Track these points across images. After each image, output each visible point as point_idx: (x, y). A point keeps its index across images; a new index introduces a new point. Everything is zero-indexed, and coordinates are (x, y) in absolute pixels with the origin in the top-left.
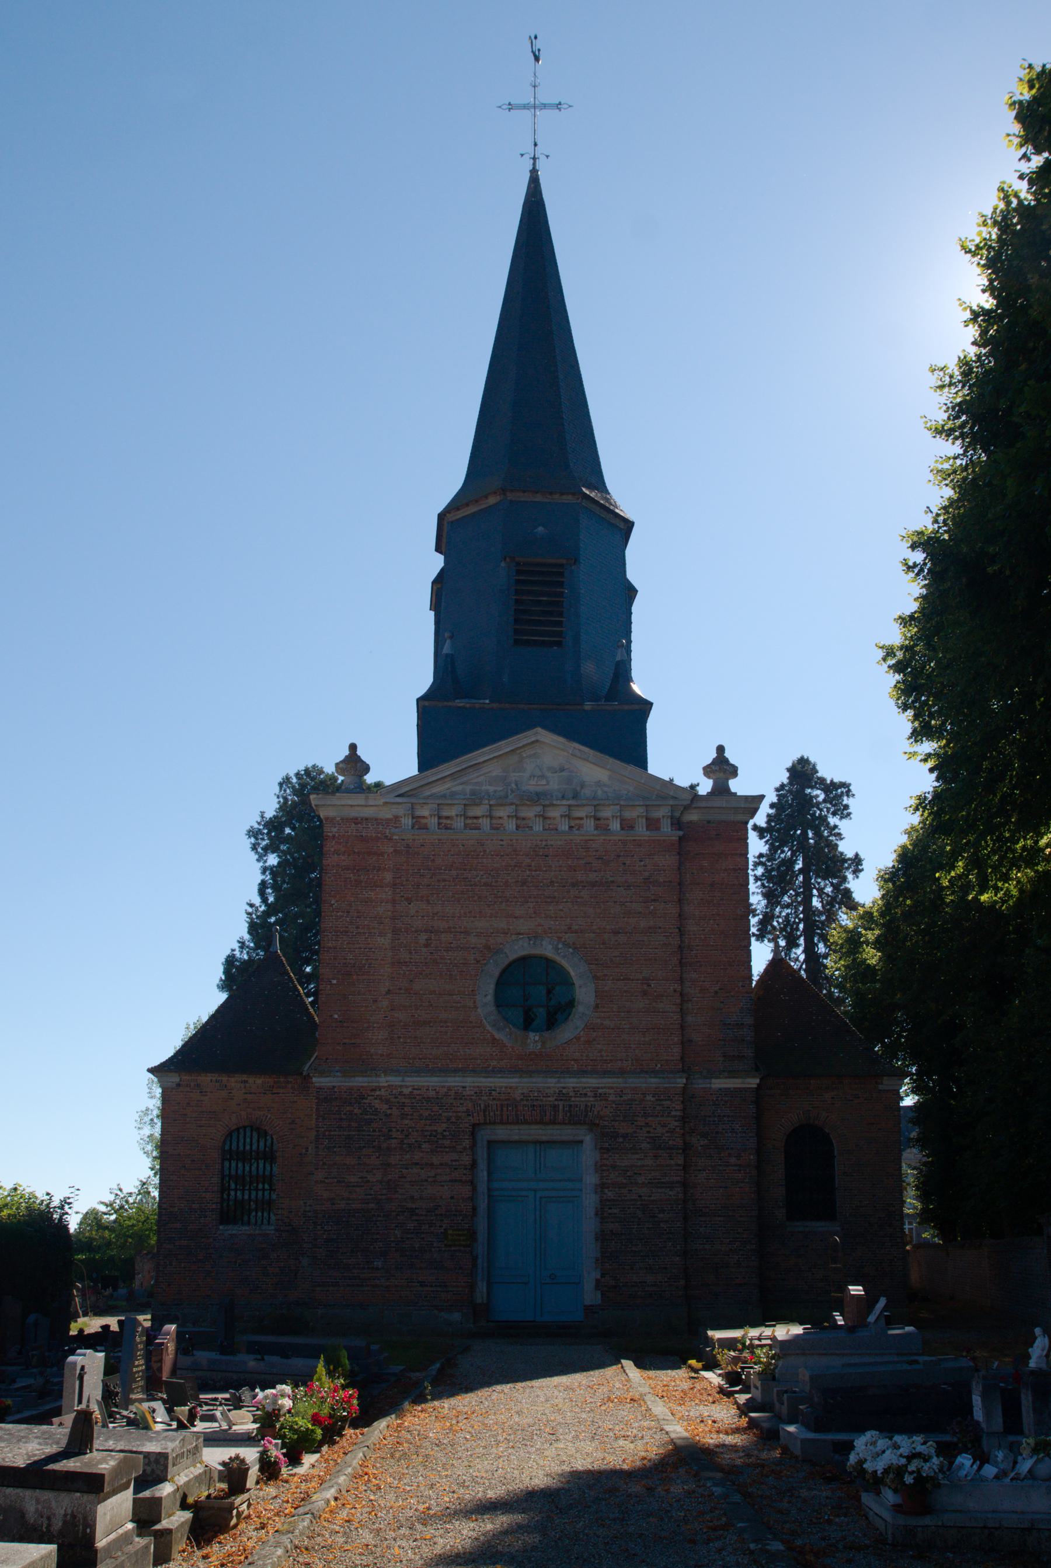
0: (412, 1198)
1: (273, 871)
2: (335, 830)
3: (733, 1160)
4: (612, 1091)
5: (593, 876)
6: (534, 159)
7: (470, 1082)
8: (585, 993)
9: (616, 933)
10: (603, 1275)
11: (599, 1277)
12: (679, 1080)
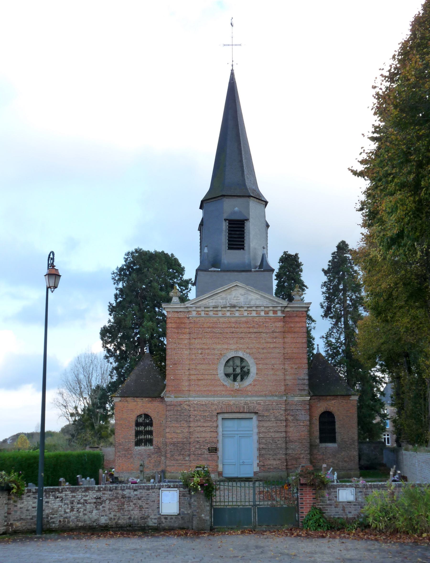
0: (198, 437)
1: (121, 290)
2: (170, 315)
3: (302, 424)
4: (262, 402)
5: (255, 330)
6: (232, 65)
7: (216, 399)
8: (253, 370)
9: (263, 349)
10: (260, 462)
11: (258, 462)
12: (284, 398)
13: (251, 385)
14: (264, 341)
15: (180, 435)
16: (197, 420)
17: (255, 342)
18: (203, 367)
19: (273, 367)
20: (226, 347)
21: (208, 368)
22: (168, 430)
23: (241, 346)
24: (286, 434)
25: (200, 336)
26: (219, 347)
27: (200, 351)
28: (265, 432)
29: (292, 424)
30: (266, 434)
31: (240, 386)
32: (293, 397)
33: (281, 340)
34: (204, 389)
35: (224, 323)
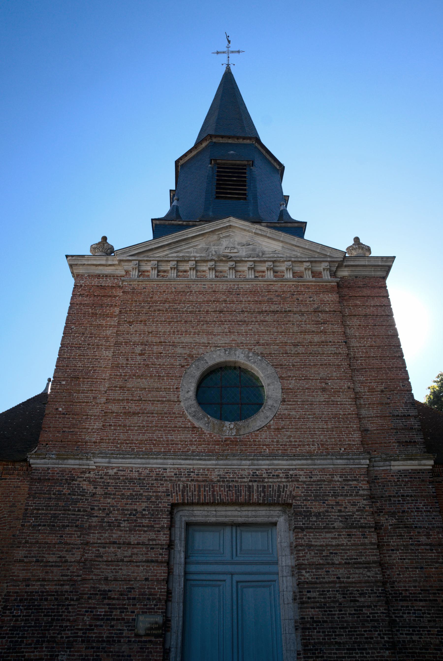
0: (106, 579)
3: (423, 539)
4: (301, 473)
5: (274, 307)
9: (295, 345)
12: (363, 461)
13: (268, 427)
14: (296, 329)
15: (55, 569)
16: (110, 524)
17: (274, 330)
18: (143, 383)
19: (323, 385)
20: (204, 340)
21: (156, 385)
22: (20, 553)
23: (242, 339)
24: (383, 573)
25: (143, 317)
26: (187, 339)
27: (138, 349)
28: (319, 566)
29: (394, 542)
30: (322, 572)
31: (238, 430)
32: (386, 460)
33: (338, 328)
34: (140, 437)
35: (200, 293)
